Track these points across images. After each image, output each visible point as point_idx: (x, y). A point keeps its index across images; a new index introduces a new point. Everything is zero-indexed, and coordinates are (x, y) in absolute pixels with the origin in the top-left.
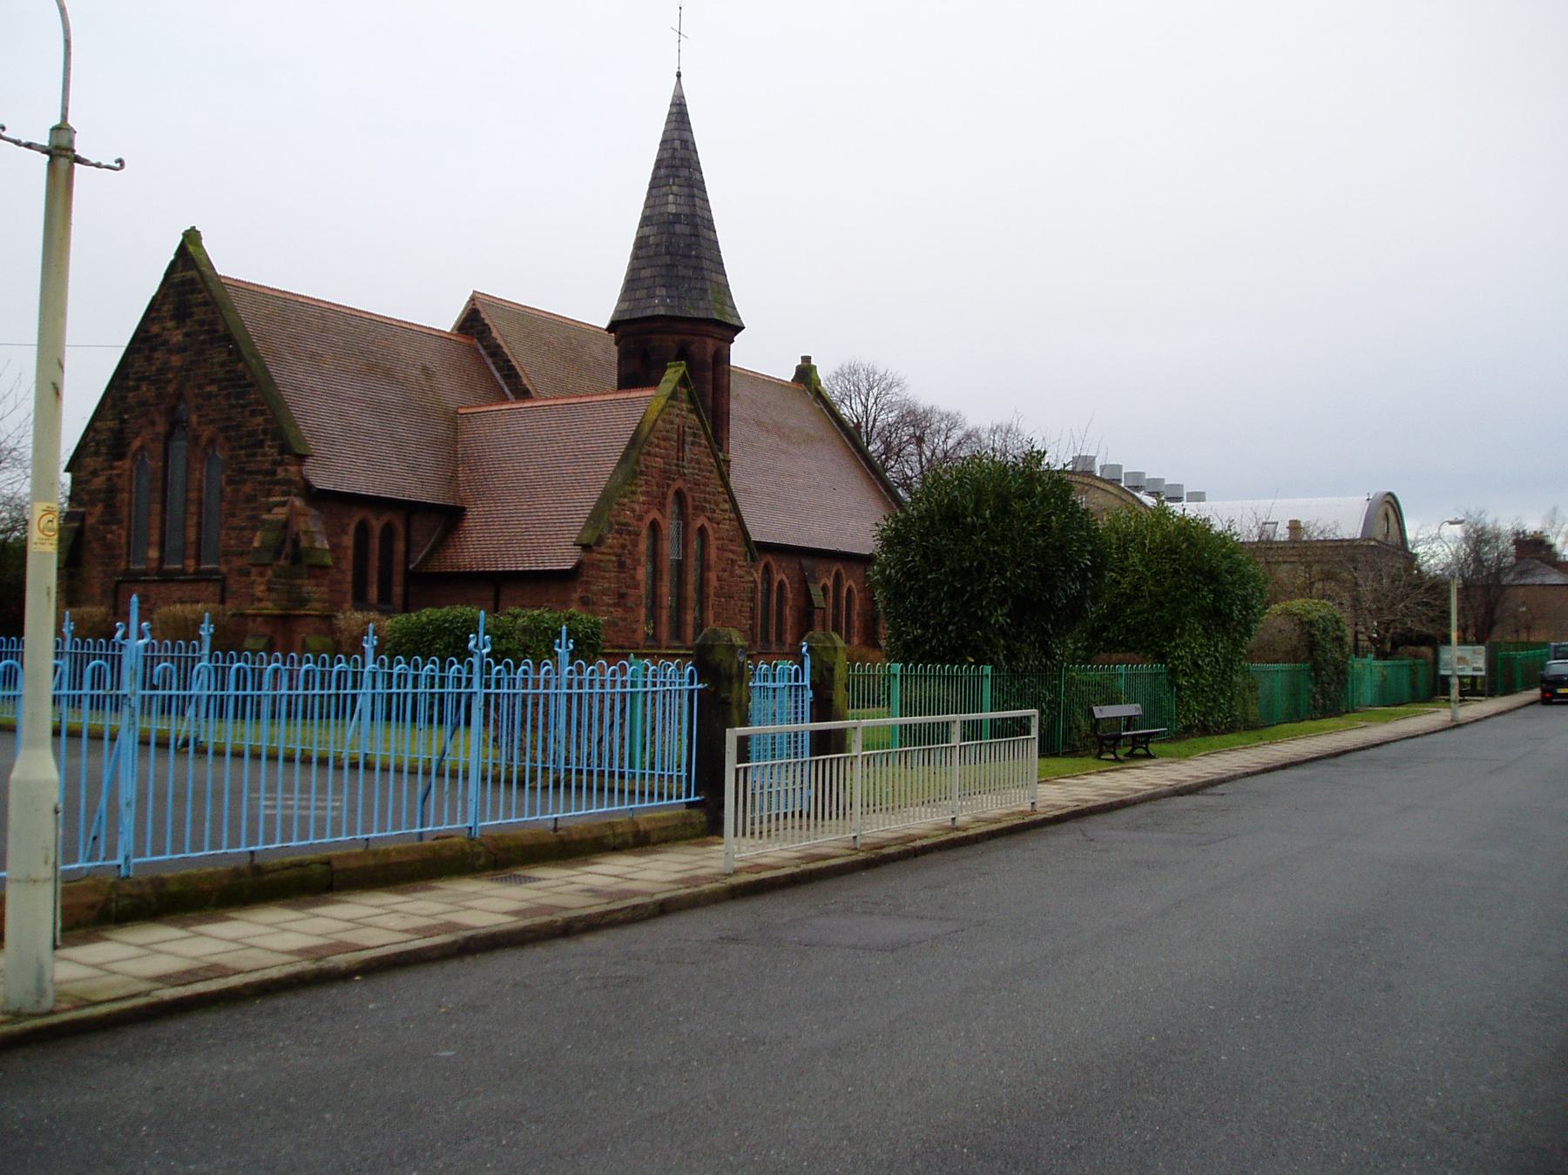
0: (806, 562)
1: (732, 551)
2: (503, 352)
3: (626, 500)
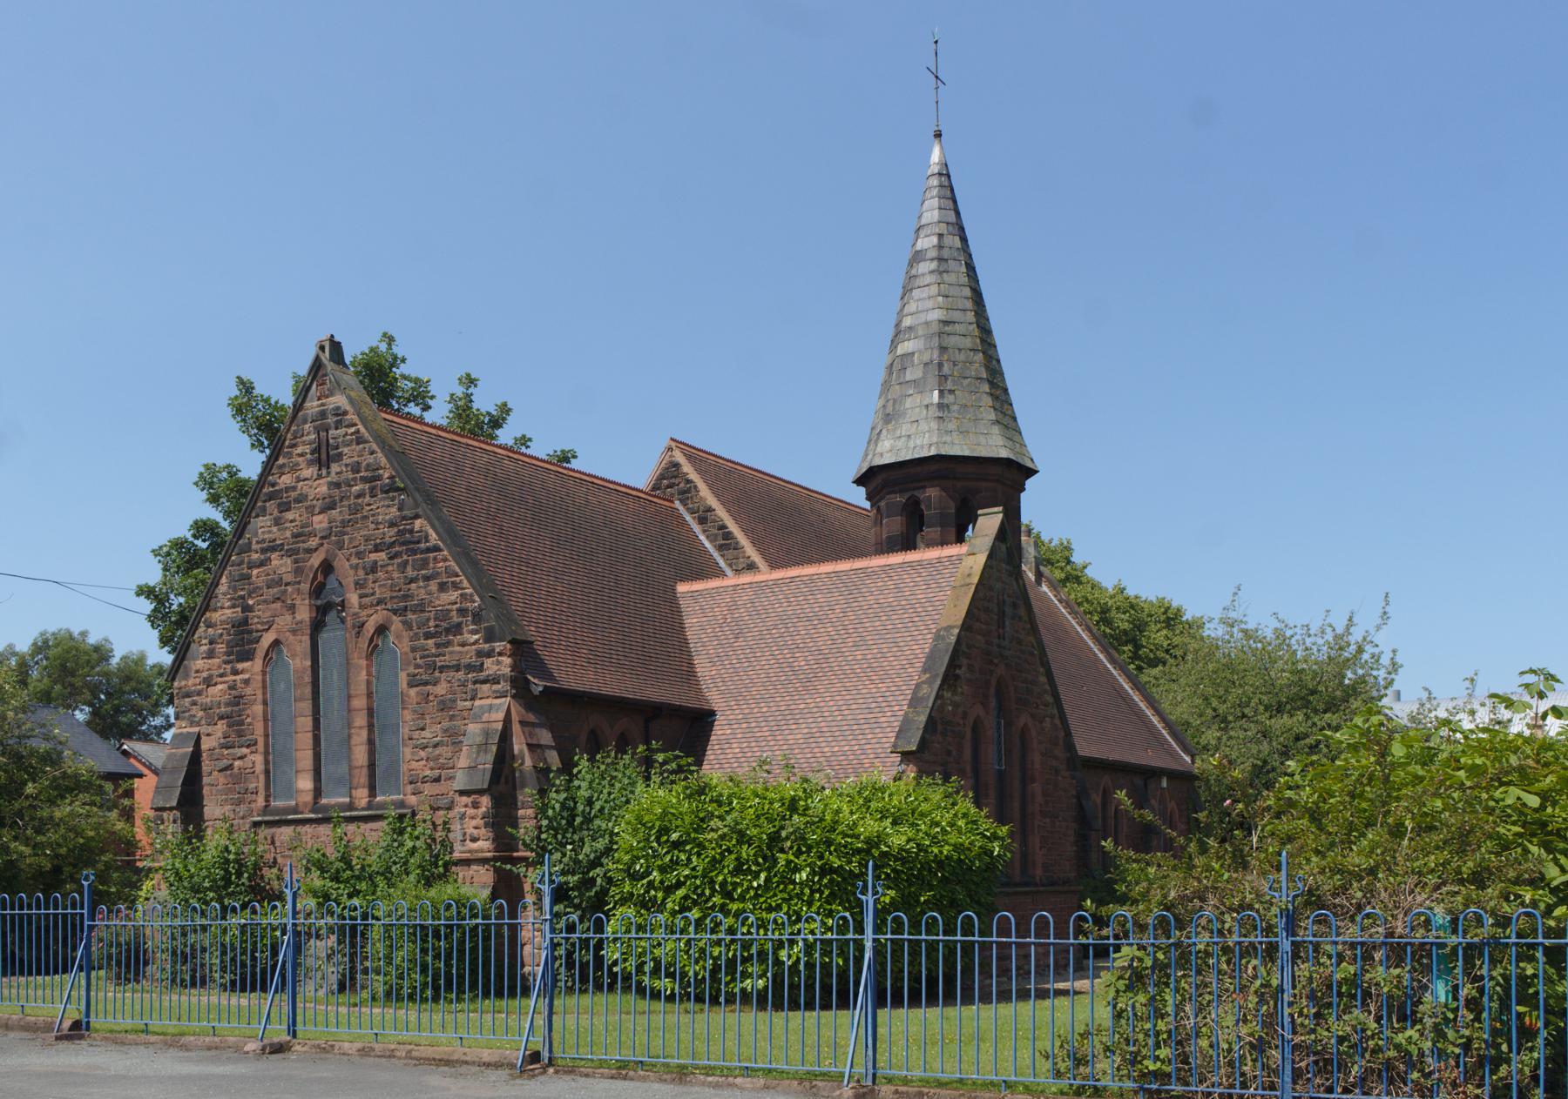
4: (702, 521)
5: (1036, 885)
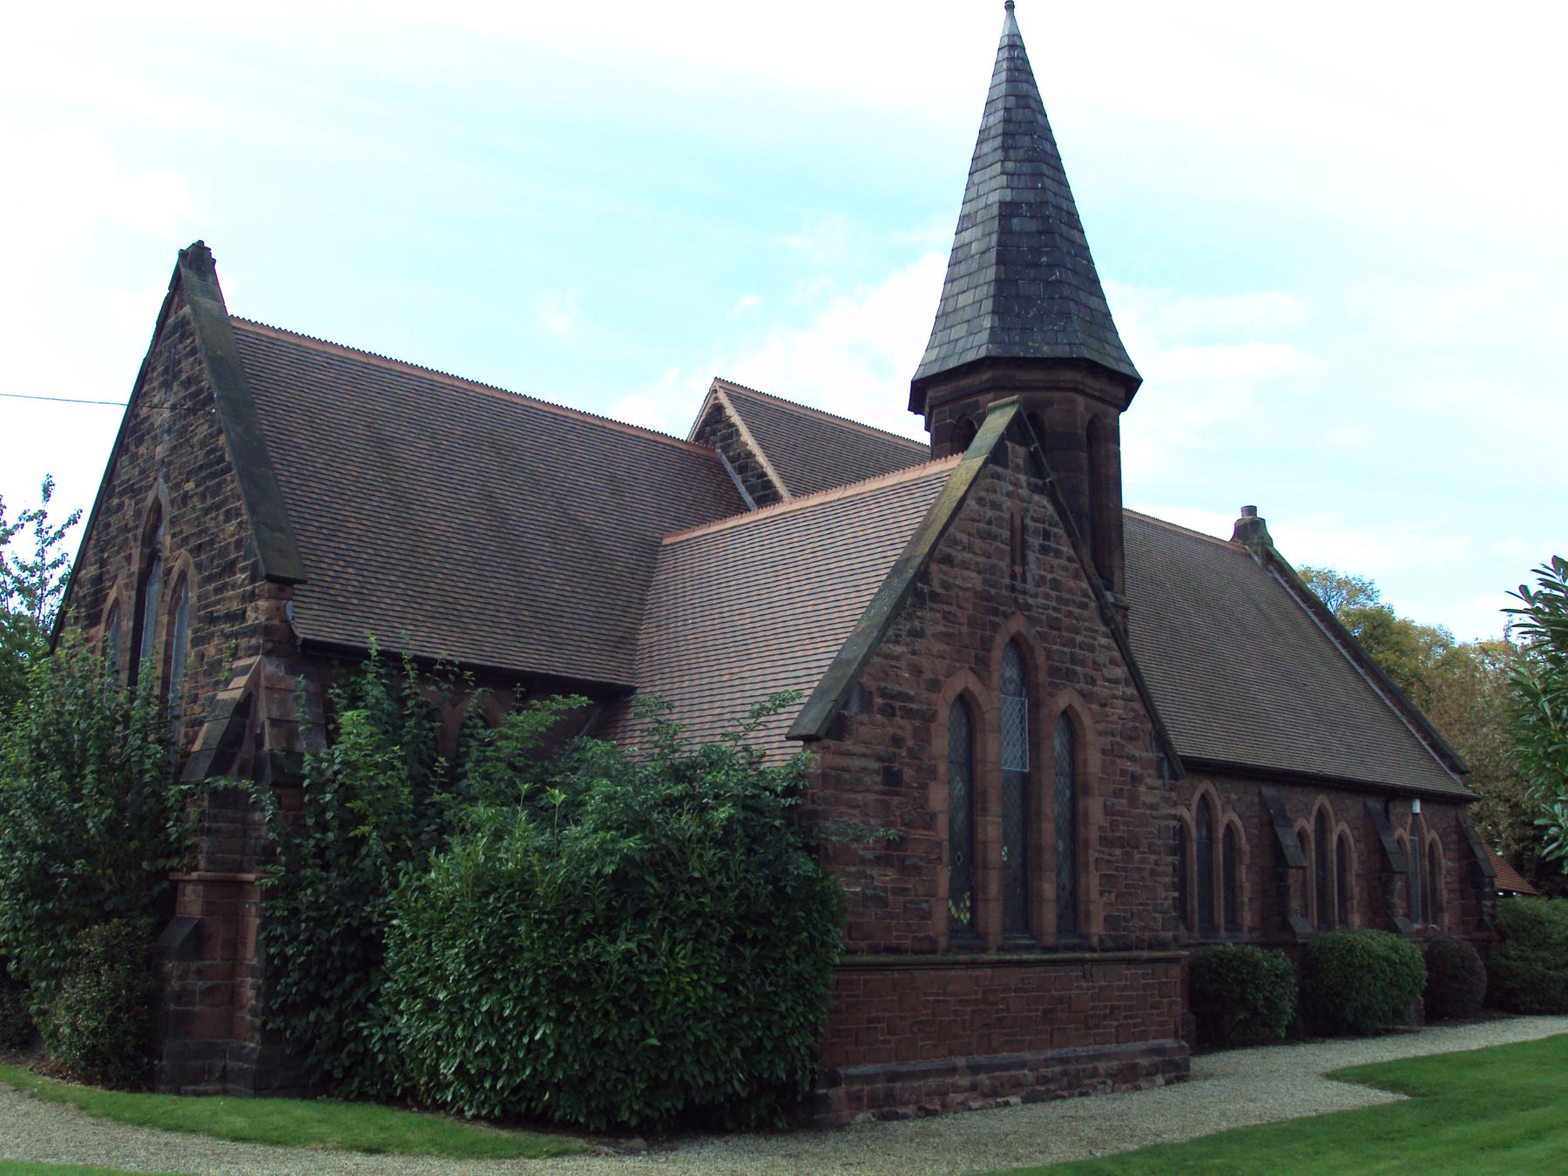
0: (1269, 792)
1: (1132, 758)
2: (757, 462)
3: (899, 649)
4: (742, 470)
5: (1093, 950)
